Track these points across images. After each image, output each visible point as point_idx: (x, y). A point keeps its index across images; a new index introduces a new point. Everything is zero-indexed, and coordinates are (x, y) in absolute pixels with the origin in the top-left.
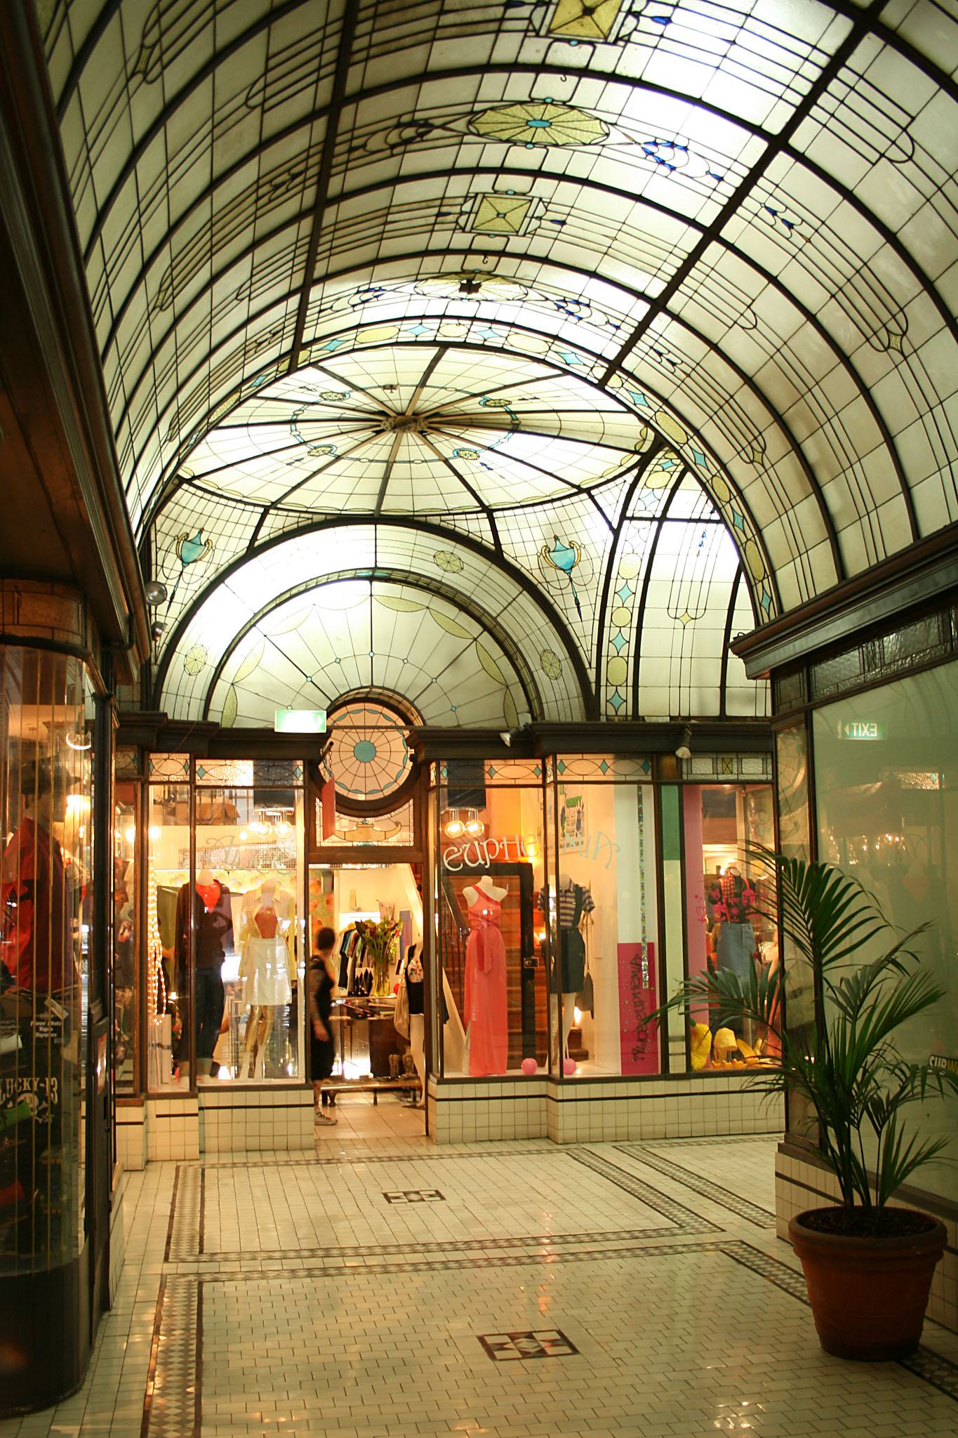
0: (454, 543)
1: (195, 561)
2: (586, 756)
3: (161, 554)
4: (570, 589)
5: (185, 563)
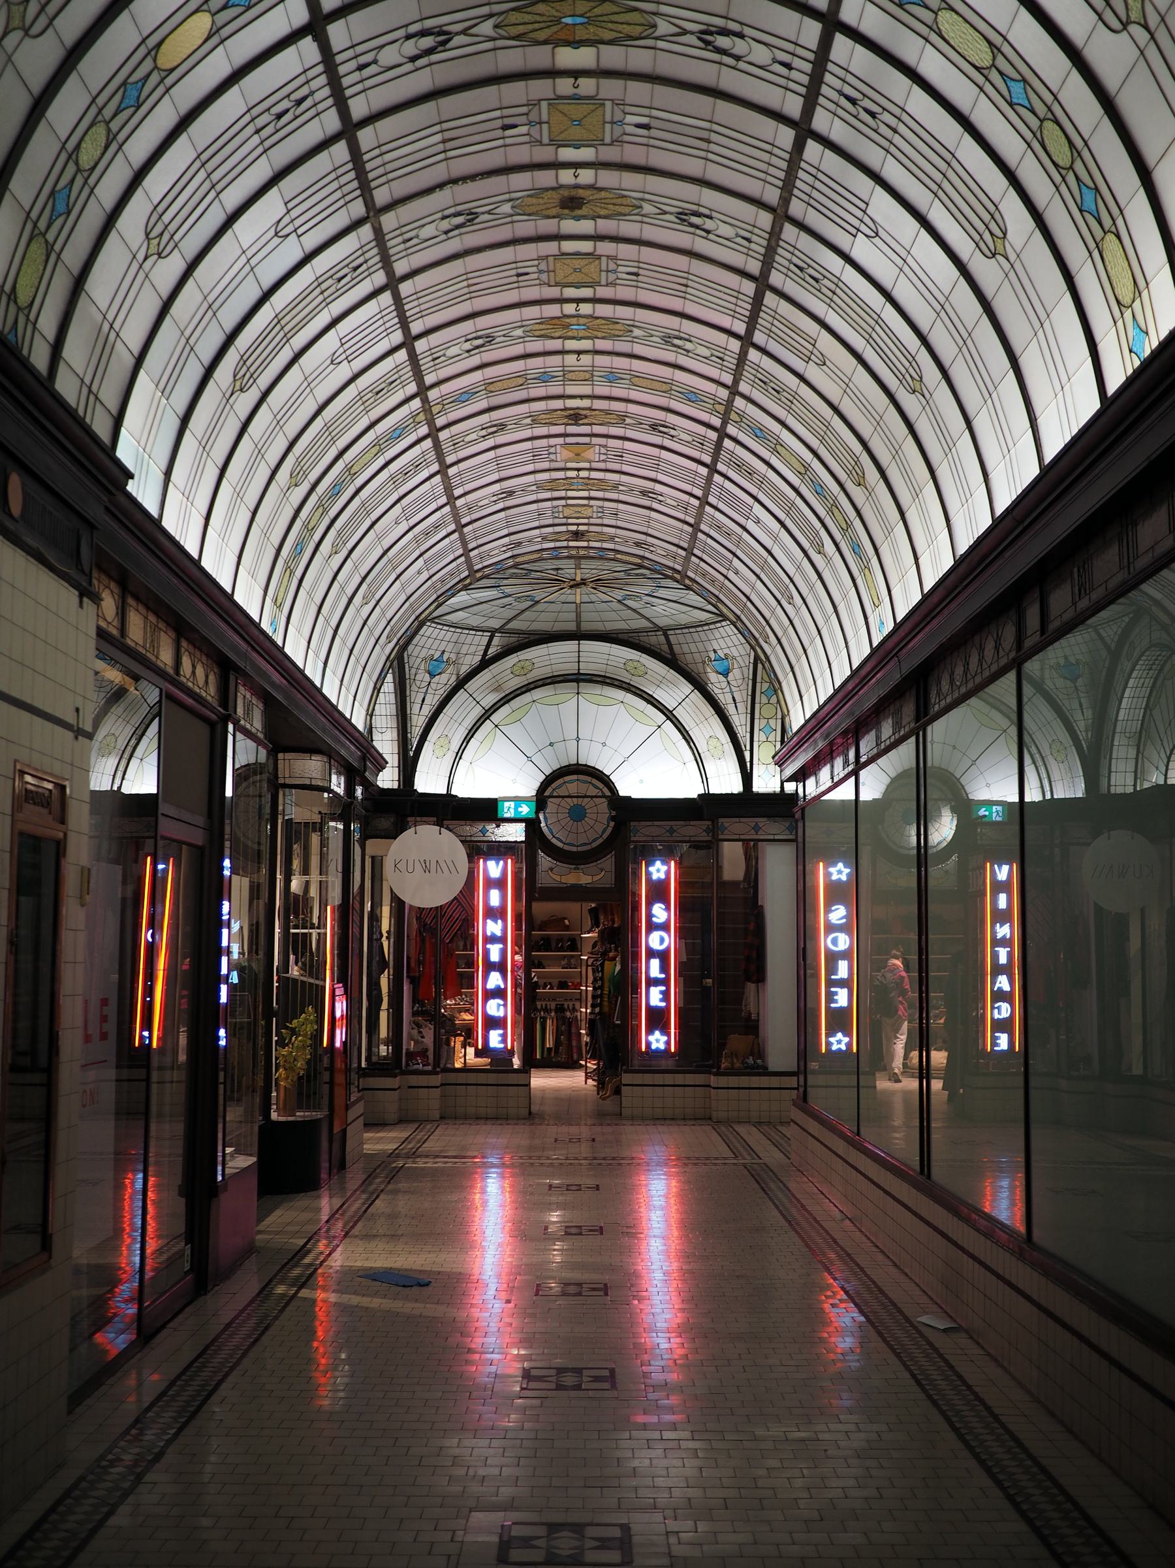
0: (640, 653)
1: (440, 674)
2: (742, 820)
3: (413, 671)
4: (728, 689)
5: (432, 676)
